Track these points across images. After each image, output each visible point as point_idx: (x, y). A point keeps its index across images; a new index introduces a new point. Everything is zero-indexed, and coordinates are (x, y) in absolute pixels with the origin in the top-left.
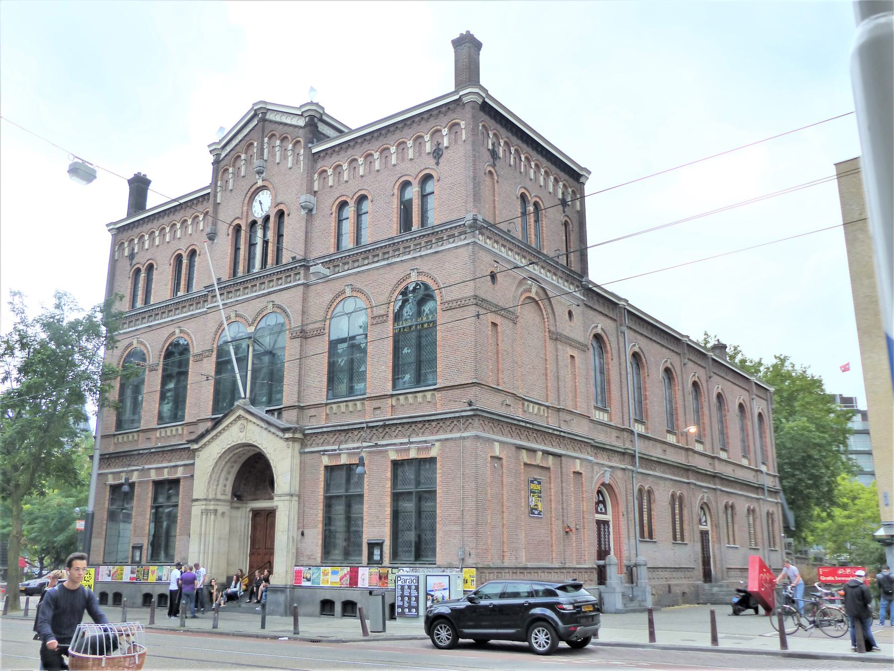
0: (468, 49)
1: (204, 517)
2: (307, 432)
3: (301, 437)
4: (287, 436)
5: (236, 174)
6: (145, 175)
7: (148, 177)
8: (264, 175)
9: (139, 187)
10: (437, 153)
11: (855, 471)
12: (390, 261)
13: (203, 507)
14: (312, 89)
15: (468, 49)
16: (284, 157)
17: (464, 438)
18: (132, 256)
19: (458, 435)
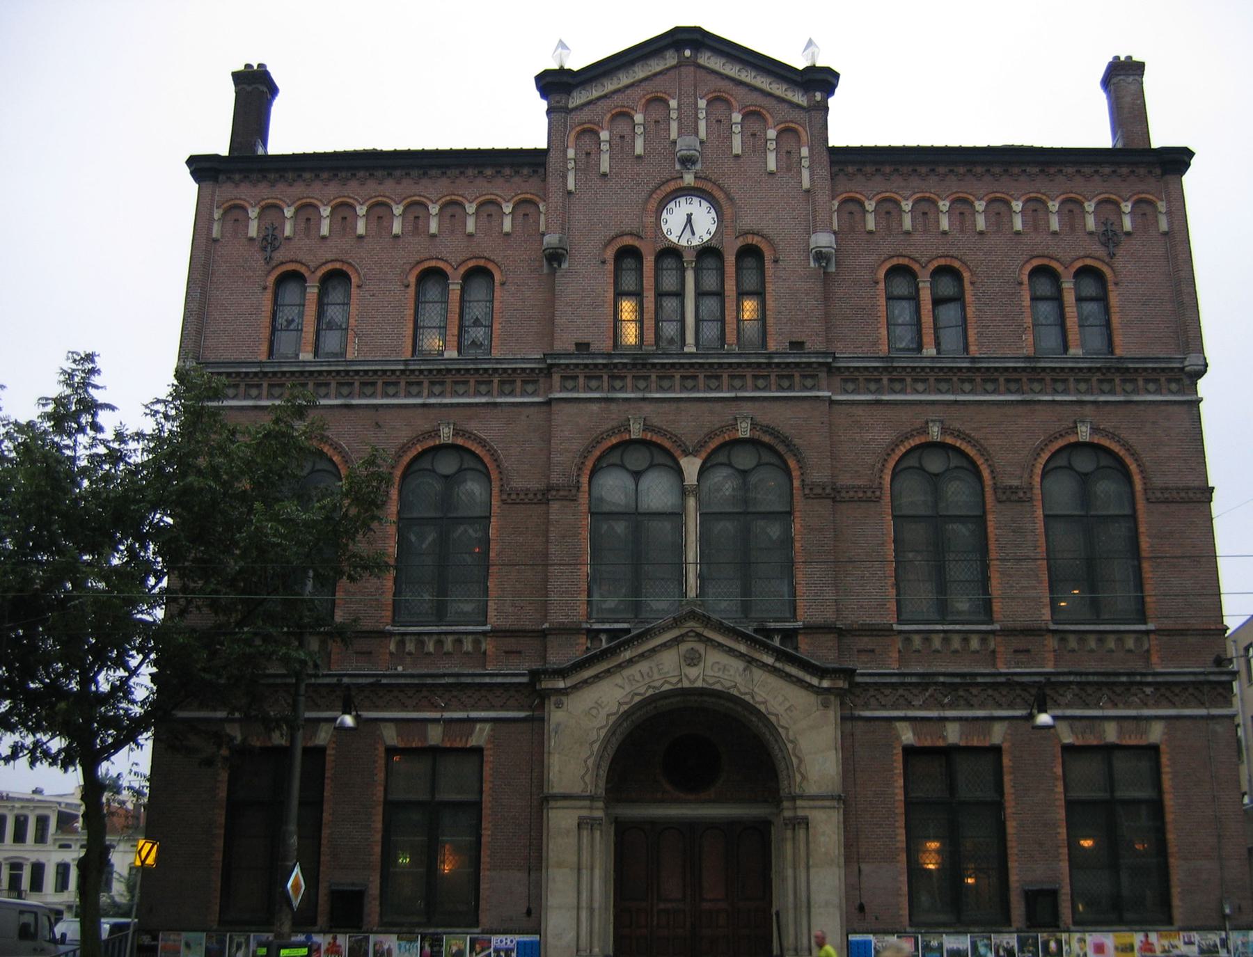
0: (1123, 79)
1: (585, 833)
2: (859, 679)
3: (846, 690)
4: (826, 684)
5: (622, 143)
6: (248, 66)
7: (1137, 58)
8: (698, 167)
9: (254, 90)
10: (1110, 237)
11: (75, 407)
12: (1028, 397)
13: (585, 813)
14: (562, 45)
15: (1123, 79)
16: (756, 144)
17: (1213, 717)
18: (270, 241)
19: (1203, 712)
